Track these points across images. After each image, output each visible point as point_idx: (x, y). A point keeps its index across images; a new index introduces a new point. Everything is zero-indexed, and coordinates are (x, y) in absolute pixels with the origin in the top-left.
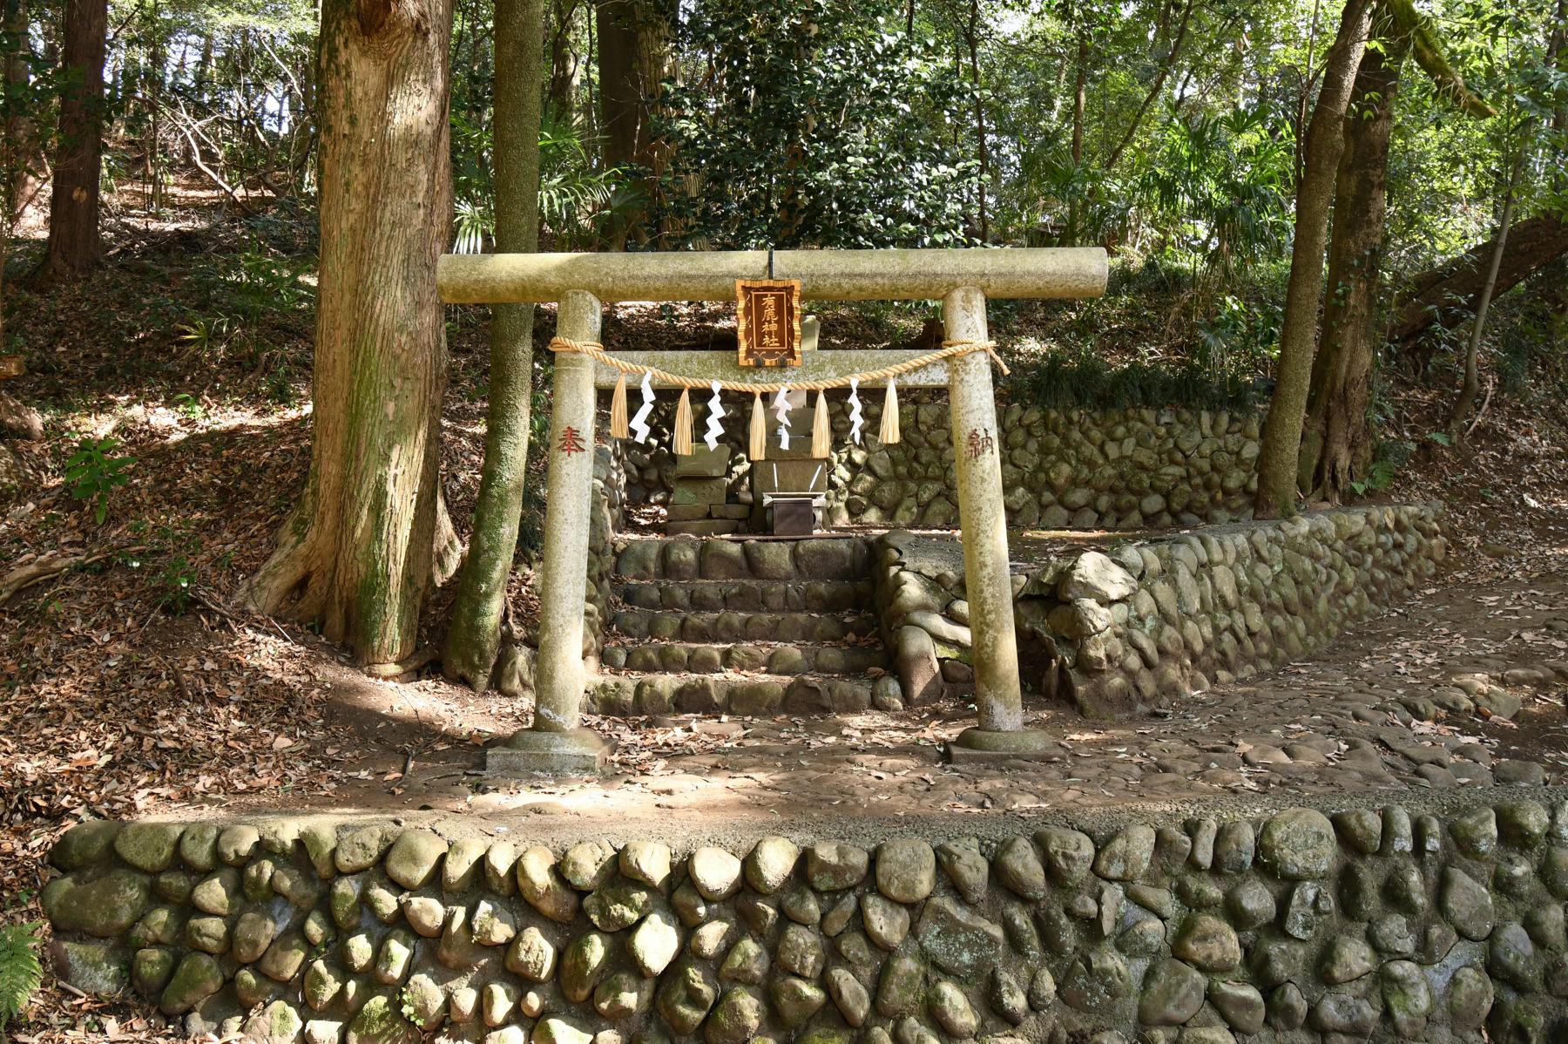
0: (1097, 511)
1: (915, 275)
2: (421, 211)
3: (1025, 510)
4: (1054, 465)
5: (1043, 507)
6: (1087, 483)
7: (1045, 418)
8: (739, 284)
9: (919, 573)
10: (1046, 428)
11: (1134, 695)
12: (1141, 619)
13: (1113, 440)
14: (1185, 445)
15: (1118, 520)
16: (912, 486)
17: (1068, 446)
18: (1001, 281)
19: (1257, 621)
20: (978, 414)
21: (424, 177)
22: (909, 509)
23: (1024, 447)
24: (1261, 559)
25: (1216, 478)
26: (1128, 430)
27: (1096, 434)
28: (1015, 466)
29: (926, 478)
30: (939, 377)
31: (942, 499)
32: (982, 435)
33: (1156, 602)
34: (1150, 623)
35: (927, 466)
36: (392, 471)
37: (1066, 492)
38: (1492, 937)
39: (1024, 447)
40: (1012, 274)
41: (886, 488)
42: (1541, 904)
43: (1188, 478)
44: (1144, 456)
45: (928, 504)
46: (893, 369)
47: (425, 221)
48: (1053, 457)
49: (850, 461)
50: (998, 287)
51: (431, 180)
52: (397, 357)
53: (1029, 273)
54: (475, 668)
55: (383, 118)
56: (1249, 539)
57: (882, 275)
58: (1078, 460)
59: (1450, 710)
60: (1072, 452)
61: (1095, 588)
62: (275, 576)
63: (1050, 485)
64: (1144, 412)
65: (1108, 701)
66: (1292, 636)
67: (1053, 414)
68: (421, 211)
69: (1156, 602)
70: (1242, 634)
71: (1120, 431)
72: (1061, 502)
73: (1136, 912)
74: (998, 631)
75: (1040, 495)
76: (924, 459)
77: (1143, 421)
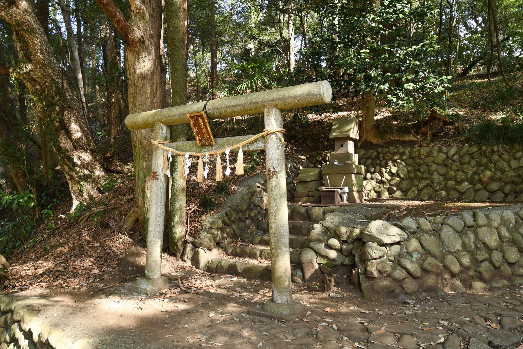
0: (504, 193)
1: (250, 104)
2: (149, 99)
3: (467, 192)
4: (483, 171)
5: (476, 191)
6: (500, 179)
7: (480, 149)
8: (188, 115)
10: (481, 155)
12: (410, 254)
13: (515, 159)
15: (516, 197)
16: (416, 182)
17: (491, 163)
18: (280, 102)
20: (271, 161)
21: (149, 88)
22: (413, 192)
23: (469, 163)
27: (506, 156)
28: (464, 172)
30: (260, 145)
31: (428, 187)
32: (272, 170)
34: (415, 256)
35: (423, 173)
36: (147, 185)
37: (488, 184)
39: (469, 163)
40: (284, 98)
41: (404, 183)
46: (242, 143)
47: (151, 103)
48: (482, 168)
50: (280, 104)
51: (152, 89)
52: (145, 148)
53: (290, 97)
54: (176, 251)
55: (135, 71)
57: (239, 105)
58: (496, 169)
60: (493, 165)
62: (131, 217)
63: (480, 181)
65: (378, 293)
67: (484, 148)
68: (149, 99)
74: (276, 257)
75: (475, 185)
76: (422, 170)
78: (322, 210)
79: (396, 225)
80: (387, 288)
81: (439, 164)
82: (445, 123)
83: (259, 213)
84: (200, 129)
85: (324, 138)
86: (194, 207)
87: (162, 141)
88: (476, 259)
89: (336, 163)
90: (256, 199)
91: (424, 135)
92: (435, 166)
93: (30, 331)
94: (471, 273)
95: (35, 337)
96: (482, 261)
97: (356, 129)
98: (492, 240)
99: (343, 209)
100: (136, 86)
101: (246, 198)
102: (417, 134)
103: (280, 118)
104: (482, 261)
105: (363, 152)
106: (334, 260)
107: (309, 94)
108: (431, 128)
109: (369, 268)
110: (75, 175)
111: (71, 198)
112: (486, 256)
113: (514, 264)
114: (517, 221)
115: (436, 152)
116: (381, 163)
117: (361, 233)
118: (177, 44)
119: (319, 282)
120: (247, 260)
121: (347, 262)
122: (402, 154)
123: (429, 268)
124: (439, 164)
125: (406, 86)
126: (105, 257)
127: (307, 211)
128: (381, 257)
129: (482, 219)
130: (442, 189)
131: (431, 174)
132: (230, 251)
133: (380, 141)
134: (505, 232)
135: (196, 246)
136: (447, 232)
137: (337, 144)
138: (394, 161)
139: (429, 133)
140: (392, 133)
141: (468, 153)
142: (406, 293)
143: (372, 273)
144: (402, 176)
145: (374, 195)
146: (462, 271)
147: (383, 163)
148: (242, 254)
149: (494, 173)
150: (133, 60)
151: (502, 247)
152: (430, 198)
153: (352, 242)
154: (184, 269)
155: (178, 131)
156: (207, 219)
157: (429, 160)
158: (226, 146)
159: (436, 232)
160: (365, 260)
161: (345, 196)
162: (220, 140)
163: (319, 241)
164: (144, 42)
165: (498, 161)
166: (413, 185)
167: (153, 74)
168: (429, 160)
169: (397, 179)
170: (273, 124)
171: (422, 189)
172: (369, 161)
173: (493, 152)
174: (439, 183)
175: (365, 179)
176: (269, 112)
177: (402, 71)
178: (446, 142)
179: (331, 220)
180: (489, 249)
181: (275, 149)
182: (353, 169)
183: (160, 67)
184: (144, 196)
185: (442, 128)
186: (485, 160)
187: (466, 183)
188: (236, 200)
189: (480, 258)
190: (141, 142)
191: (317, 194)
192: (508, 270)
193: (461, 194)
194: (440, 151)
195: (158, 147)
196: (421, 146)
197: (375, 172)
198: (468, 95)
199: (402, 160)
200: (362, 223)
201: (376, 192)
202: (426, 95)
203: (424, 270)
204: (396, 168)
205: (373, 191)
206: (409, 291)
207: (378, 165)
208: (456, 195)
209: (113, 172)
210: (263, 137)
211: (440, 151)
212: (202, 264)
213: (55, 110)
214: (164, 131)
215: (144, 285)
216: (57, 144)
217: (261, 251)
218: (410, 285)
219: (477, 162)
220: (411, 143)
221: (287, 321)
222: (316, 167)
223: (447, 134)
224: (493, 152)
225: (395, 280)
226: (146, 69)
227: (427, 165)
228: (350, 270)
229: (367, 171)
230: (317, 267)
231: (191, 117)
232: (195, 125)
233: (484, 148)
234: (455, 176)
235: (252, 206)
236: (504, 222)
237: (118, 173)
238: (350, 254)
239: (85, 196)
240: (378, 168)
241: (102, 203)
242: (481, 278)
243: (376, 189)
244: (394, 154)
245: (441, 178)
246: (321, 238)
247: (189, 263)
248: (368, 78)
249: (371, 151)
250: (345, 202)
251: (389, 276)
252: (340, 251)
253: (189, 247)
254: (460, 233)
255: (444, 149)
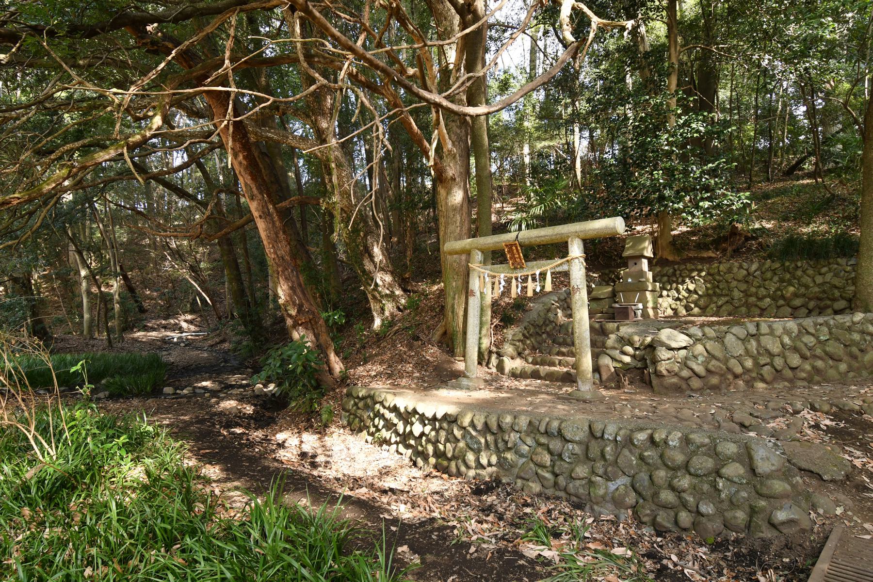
4: (785, 287)
5: (778, 307)
7: (783, 265)
12: (695, 357)
16: (715, 299)
17: (795, 278)
23: (771, 279)
26: (830, 269)
27: (810, 272)
29: (722, 295)
30: (565, 268)
34: (701, 359)
35: (722, 290)
37: (791, 300)
38: (633, 477)
39: (771, 279)
42: (657, 469)
44: (836, 282)
45: (721, 306)
46: (549, 266)
49: (687, 289)
50: (582, 235)
51: (461, 219)
55: (446, 204)
59: (841, 409)
63: (783, 297)
64: (839, 260)
65: (667, 388)
67: (787, 264)
71: (824, 270)
72: (789, 305)
73: (521, 442)
75: (777, 301)
76: (721, 287)
77: (838, 264)
78: (616, 325)
79: (683, 333)
80: (674, 384)
81: (739, 281)
82: (747, 239)
83: (554, 328)
84: (513, 254)
85: (616, 256)
86: (496, 322)
87: (478, 265)
88: (758, 363)
89: (630, 280)
90: (551, 315)
91: (724, 251)
92: (735, 282)
93: (395, 406)
94: (754, 375)
95: (402, 410)
96: (764, 365)
97: (650, 247)
98: (776, 348)
99: (636, 323)
100: (447, 217)
101: (542, 314)
102: (717, 250)
103: (582, 246)
104: (764, 365)
105: (658, 269)
106: (628, 364)
107: (606, 228)
108: (731, 244)
109: (658, 368)
110: (378, 295)
111: (373, 317)
112: (768, 360)
113: (796, 368)
114: (800, 331)
115: (738, 268)
116: (677, 279)
117: (653, 340)
118: (484, 180)
119: (616, 380)
120: (547, 367)
121: (639, 365)
122: (701, 271)
123: (713, 369)
124: (739, 281)
125: (701, 204)
126: (422, 364)
127: (601, 326)
128: (669, 359)
129: (764, 328)
130: (743, 306)
131: (730, 290)
132: (530, 360)
133: (676, 257)
134: (786, 340)
135: (499, 355)
136: (730, 339)
137: (631, 263)
138: (692, 278)
139: (730, 249)
140: (689, 250)
141: (770, 269)
142: (692, 390)
143: (661, 372)
144: (700, 293)
145: (670, 312)
146: (744, 373)
147: (680, 280)
148: (543, 363)
149: (798, 289)
150: (445, 195)
151: (784, 354)
152: (730, 315)
153: (644, 349)
154: (491, 374)
155: (497, 256)
156: (510, 332)
157: (729, 277)
158: (536, 268)
159: (720, 339)
160: (655, 362)
161: (639, 312)
162: (530, 264)
163: (614, 348)
164: (455, 179)
165: (802, 277)
166: (712, 302)
167: (462, 206)
168: (729, 277)
169: (696, 296)
170: (576, 250)
171: (721, 306)
172: (665, 279)
173: (797, 267)
174: (740, 300)
175: (661, 296)
176: (572, 241)
177: (697, 190)
178: (747, 258)
179: (625, 330)
180: (771, 355)
181: (578, 272)
182: (648, 287)
183: (469, 200)
184: (453, 312)
185: (744, 243)
186: (788, 276)
187: (768, 299)
188: (533, 315)
189: (762, 362)
190: (451, 265)
191: (611, 311)
192: (788, 373)
193: (763, 310)
194: (741, 267)
195: (474, 270)
196: (720, 263)
197: (671, 289)
198: (783, 204)
199: (700, 277)
200: (653, 334)
201: (672, 309)
202: (724, 212)
203: (708, 371)
204: (694, 286)
205: (669, 309)
206: (694, 388)
207: (674, 282)
208: (758, 311)
209: (409, 291)
210: (568, 261)
211: (741, 267)
212: (507, 370)
213: (359, 235)
214: (478, 256)
215: (464, 382)
216: (362, 265)
217: (560, 361)
218: (696, 383)
219: (779, 278)
220: (710, 260)
221: (591, 402)
222: (608, 284)
223: (749, 249)
224: (797, 267)
225: (682, 378)
226: (457, 202)
227: (727, 282)
228: (643, 372)
229: (663, 288)
230: (613, 370)
231: (506, 246)
232: (509, 252)
233: (787, 264)
234: (757, 293)
235: (547, 322)
236: (787, 332)
237: (415, 292)
238: (643, 359)
239: (387, 313)
240: (674, 285)
241: (403, 319)
242: (763, 380)
243: (673, 306)
244: (692, 270)
245: (742, 295)
246: (616, 346)
247: (494, 370)
248: (662, 198)
249: (667, 268)
250: (640, 318)
251: (676, 374)
252: (633, 357)
253: (494, 357)
254: (743, 340)
255: (745, 265)
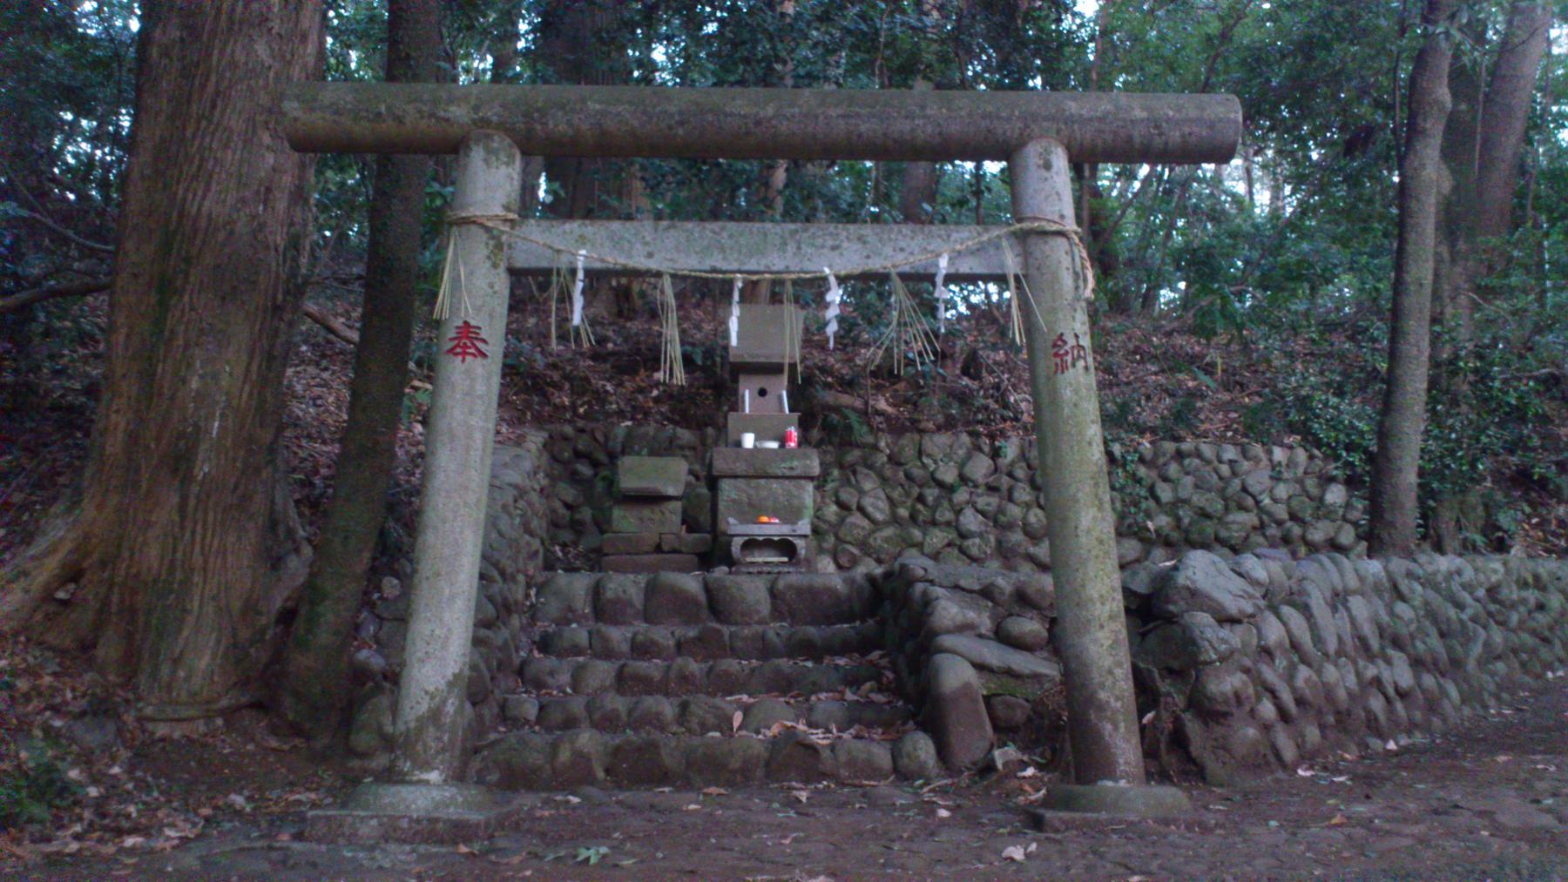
9: (957, 587)
11: (1272, 759)
14: (1255, 488)
16: (917, 533)
19: (1406, 678)
24: (1402, 597)
25: (1296, 530)
29: (934, 523)
33: (1288, 631)
35: (934, 509)
43: (1261, 527)
56: (1385, 568)
61: (1208, 597)
66: (1446, 703)
69: (1288, 631)
70: (1391, 691)
76: (930, 499)
